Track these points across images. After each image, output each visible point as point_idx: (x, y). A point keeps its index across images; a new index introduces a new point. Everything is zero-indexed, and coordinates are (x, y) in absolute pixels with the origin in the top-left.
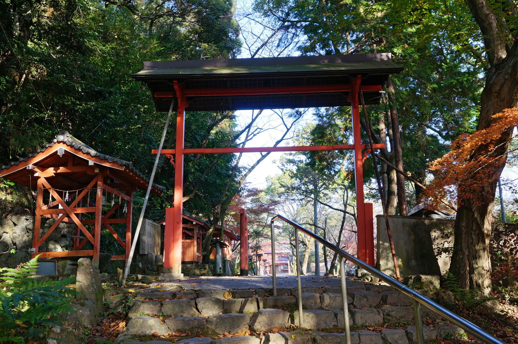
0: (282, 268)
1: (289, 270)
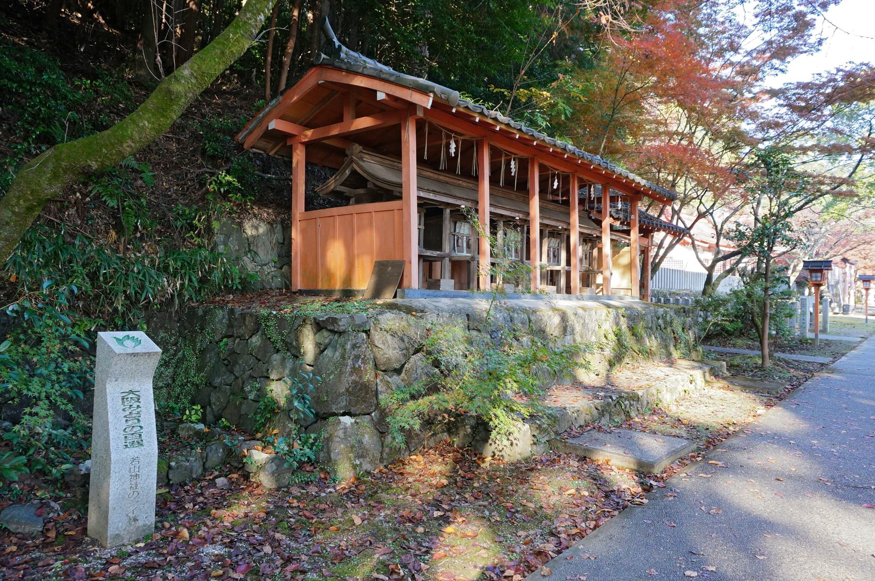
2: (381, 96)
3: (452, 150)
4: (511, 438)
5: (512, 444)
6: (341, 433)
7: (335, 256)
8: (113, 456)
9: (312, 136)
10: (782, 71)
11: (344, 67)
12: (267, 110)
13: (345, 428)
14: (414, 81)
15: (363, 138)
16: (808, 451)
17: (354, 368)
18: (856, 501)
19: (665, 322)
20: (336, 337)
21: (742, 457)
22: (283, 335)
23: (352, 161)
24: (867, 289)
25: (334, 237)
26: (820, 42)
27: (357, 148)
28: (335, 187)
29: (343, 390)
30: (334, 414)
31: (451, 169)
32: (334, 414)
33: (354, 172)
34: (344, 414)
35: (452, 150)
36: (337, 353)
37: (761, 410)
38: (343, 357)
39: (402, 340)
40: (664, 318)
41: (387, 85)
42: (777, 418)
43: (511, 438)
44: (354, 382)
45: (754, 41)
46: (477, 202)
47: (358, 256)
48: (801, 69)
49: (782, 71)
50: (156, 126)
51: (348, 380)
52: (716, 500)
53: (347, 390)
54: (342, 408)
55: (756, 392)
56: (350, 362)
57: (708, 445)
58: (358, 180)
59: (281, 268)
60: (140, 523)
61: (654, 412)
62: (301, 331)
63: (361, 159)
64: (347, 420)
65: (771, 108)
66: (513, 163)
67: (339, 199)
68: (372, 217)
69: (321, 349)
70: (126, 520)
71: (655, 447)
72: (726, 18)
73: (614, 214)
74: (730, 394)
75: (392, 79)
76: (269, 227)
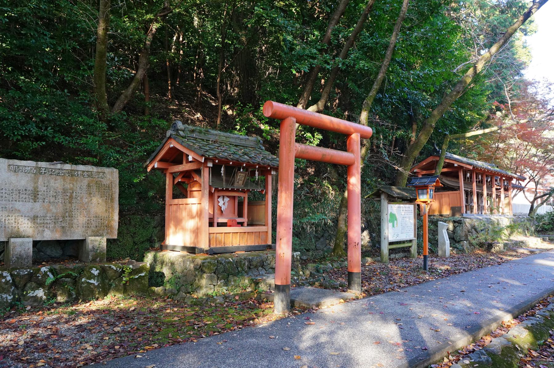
2: (456, 165)
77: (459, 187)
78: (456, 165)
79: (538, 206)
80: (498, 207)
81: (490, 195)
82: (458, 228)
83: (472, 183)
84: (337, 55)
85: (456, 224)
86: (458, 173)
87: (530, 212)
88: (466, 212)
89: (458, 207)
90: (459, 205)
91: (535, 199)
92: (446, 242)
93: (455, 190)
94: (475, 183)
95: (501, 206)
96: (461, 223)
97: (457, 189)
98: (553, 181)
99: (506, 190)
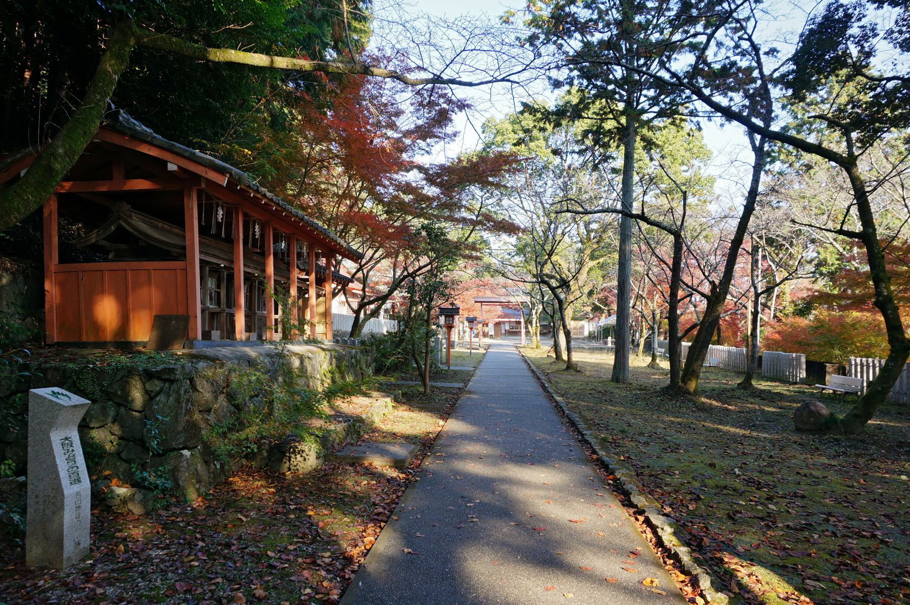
0: (507, 328)
1: (523, 331)
2: (172, 167)
3: (220, 217)
4: (304, 455)
5: (305, 460)
6: (185, 464)
7: (107, 311)
8: (66, 492)
9: (70, 188)
10: (427, 152)
11: (129, 132)
12: (19, 156)
13: (187, 460)
14: (211, 161)
15: (139, 200)
16: (487, 442)
17: (186, 410)
18: (524, 462)
19: (357, 361)
20: (167, 385)
21: (453, 450)
22: (103, 386)
23: (119, 218)
24: (471, 329)
25: (103, 292)
26: (455, 135)
27: (126, 207)
28: (97, 241)
29: (180, 429)
30: (174, 449)
31: (217, 236)
32: (174, 449)
33: (120, 229)
34: (183, 448)
35: (220, 217)
36: (171, 398)
37: (441, 423)
38: (178, 400)
39: (212, 384)
40: (355, 357)
41: (179, 158)
42: (453, 426)
43: (304, 455)
44: (188, 421)
45: (407, 122)
46: (233, 262)
47: (133, 309)
48: (439, 154)
49: (427, 152)
50: (38, 200)
51: (183, 420)
52: (456, 473)
53: (184, 428)
54: (180, 444)
55: (430, 411)
56: (184, 405)
57: (426, 445)
58: (122, 235)
59: (24, 320)
60: (82, 546)
61: (373, 432)
62: (127, 382)
63: (131, 217)
64: (186, 453)
65: (413, 177)
66: (257, 227)
67: (94, 253)
68: (150, 274)
69: (150, 397)
70: (73, 544)
71: (400, 451)
72: (389, 101)
73: (301, 266)
74: (412, 414)
75: (187, 154)
76: (11, 276)
77: (184, 248)
78: (172, 167)
79: (365, 320)
80: (302, 322)
81: (282, 289)
82: (161, 398)
83: (263, 254)
84: (426, 243)
85: (156, 385)
86: (180, 196)
87: (353, 330)
88: (206, 336)
89: (177, 318)
90: (181, 312)
91: (362, 306)
92: (69, 490)
93: (175, 259)
94: (272, 256)
95: (308, 317)
96: (172, 382)
97: (180, 254)
98: (908, 592)
99: (320, 282)
